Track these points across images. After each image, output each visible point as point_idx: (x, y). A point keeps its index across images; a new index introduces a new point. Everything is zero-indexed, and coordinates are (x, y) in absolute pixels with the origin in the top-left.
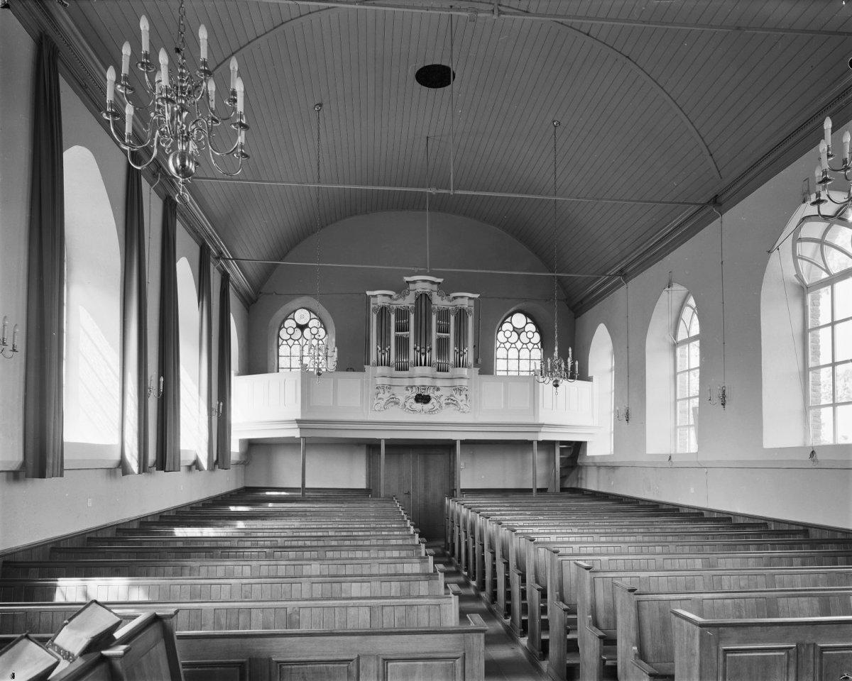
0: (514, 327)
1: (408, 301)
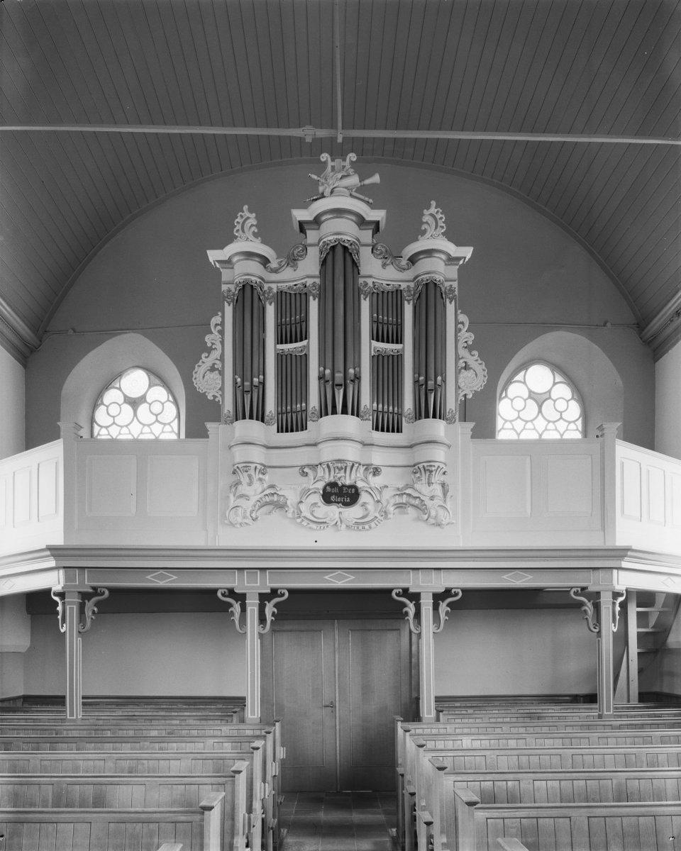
0: (530, 392)
1: (308, 269)
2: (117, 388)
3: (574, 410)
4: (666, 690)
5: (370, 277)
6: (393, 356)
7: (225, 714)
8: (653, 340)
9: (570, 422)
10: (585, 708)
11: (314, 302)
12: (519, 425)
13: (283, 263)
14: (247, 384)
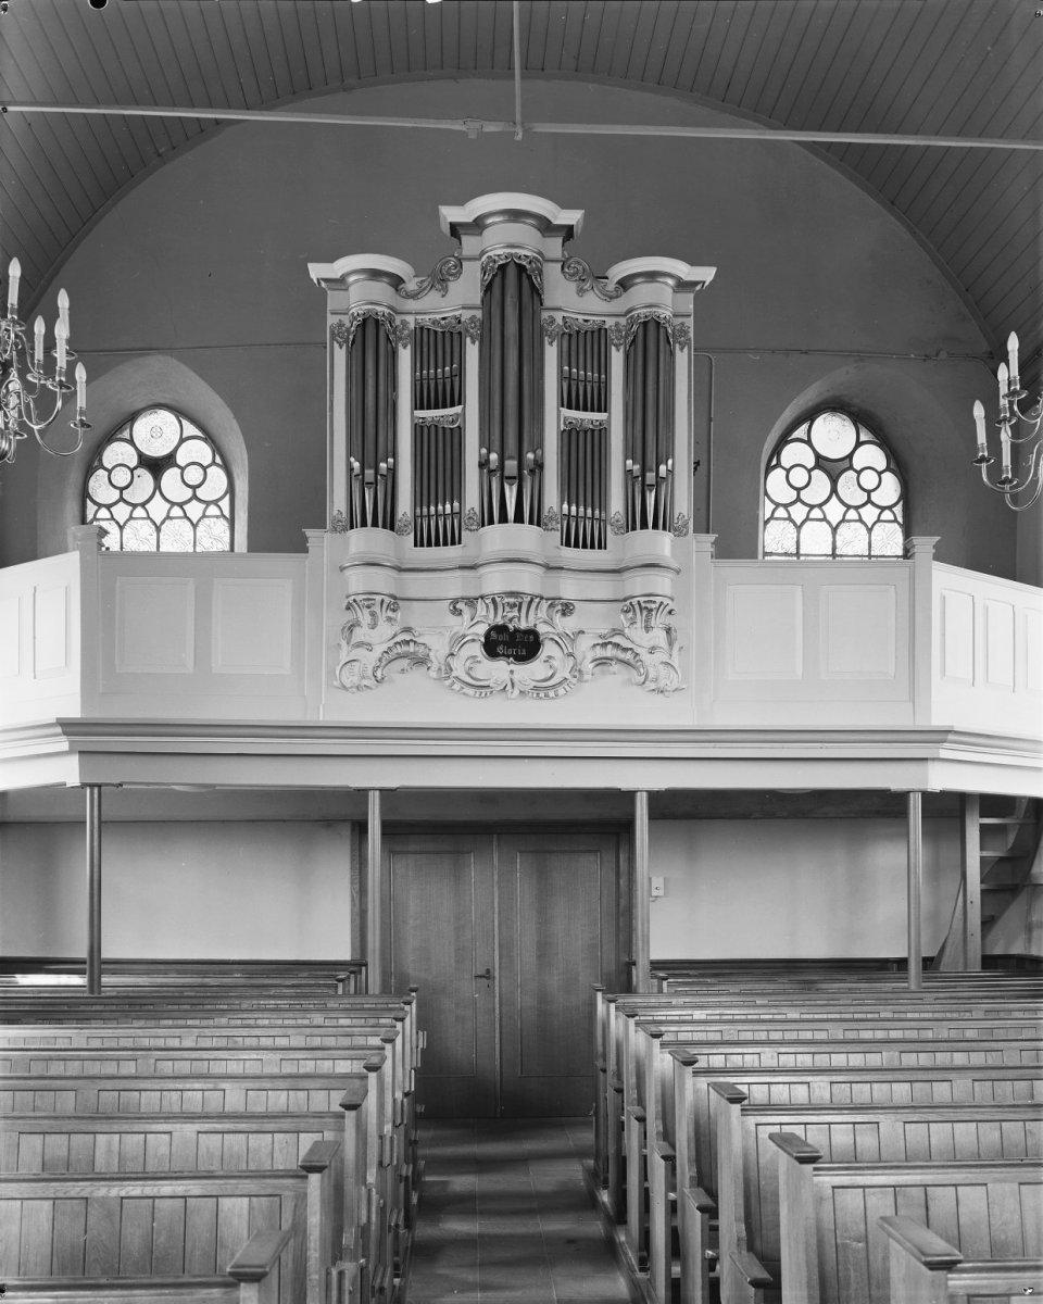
0: (818, 456)
1: (462, 297)
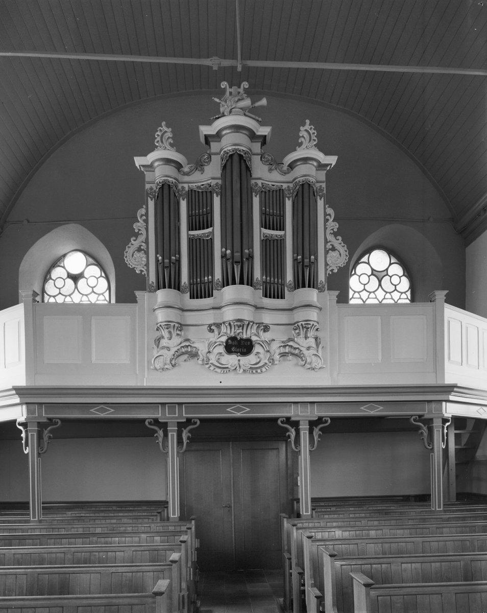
0: (373, 270)
1: (211, 174)
2: (61, 266)
3: (405, 284)
4: (475, 491)
5: (259, 179)
6: (277, 240)
7: (150, 514)
8: (464, 230)
9: (402, 293)
10: (418, 505)
11: (217, 198)
12: (364, 295)
13: (193, 167)
14: (167, 261)
